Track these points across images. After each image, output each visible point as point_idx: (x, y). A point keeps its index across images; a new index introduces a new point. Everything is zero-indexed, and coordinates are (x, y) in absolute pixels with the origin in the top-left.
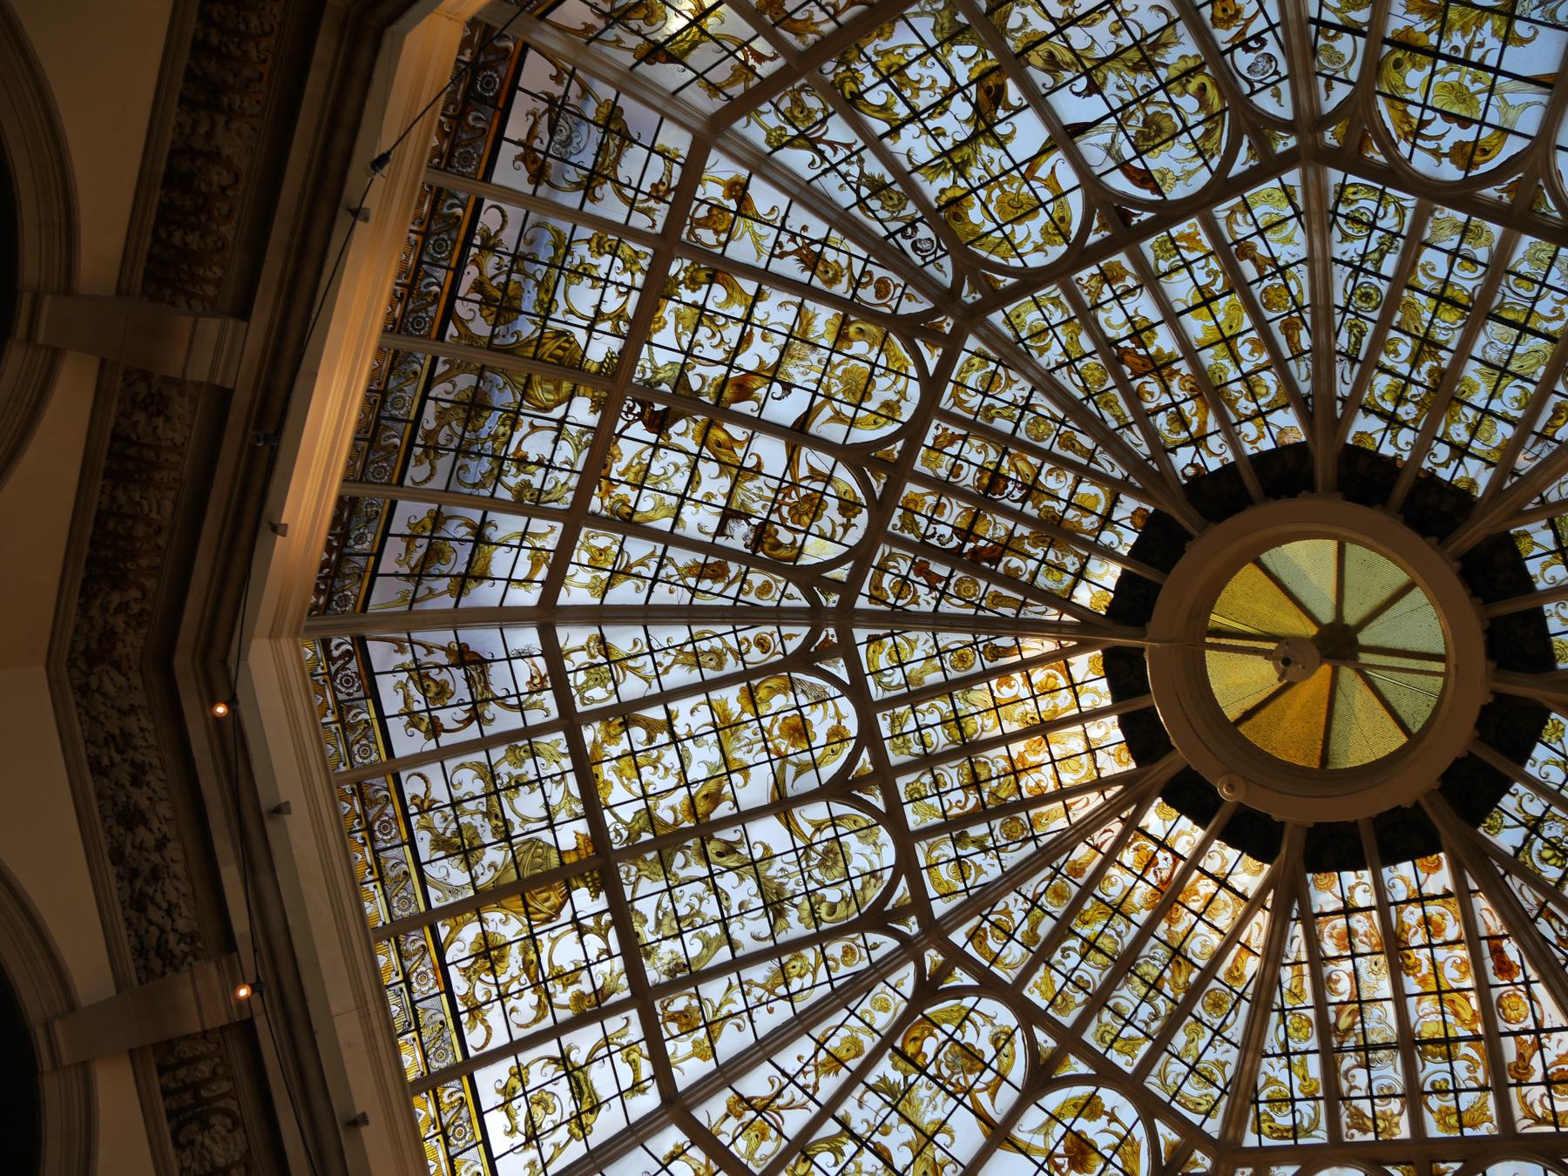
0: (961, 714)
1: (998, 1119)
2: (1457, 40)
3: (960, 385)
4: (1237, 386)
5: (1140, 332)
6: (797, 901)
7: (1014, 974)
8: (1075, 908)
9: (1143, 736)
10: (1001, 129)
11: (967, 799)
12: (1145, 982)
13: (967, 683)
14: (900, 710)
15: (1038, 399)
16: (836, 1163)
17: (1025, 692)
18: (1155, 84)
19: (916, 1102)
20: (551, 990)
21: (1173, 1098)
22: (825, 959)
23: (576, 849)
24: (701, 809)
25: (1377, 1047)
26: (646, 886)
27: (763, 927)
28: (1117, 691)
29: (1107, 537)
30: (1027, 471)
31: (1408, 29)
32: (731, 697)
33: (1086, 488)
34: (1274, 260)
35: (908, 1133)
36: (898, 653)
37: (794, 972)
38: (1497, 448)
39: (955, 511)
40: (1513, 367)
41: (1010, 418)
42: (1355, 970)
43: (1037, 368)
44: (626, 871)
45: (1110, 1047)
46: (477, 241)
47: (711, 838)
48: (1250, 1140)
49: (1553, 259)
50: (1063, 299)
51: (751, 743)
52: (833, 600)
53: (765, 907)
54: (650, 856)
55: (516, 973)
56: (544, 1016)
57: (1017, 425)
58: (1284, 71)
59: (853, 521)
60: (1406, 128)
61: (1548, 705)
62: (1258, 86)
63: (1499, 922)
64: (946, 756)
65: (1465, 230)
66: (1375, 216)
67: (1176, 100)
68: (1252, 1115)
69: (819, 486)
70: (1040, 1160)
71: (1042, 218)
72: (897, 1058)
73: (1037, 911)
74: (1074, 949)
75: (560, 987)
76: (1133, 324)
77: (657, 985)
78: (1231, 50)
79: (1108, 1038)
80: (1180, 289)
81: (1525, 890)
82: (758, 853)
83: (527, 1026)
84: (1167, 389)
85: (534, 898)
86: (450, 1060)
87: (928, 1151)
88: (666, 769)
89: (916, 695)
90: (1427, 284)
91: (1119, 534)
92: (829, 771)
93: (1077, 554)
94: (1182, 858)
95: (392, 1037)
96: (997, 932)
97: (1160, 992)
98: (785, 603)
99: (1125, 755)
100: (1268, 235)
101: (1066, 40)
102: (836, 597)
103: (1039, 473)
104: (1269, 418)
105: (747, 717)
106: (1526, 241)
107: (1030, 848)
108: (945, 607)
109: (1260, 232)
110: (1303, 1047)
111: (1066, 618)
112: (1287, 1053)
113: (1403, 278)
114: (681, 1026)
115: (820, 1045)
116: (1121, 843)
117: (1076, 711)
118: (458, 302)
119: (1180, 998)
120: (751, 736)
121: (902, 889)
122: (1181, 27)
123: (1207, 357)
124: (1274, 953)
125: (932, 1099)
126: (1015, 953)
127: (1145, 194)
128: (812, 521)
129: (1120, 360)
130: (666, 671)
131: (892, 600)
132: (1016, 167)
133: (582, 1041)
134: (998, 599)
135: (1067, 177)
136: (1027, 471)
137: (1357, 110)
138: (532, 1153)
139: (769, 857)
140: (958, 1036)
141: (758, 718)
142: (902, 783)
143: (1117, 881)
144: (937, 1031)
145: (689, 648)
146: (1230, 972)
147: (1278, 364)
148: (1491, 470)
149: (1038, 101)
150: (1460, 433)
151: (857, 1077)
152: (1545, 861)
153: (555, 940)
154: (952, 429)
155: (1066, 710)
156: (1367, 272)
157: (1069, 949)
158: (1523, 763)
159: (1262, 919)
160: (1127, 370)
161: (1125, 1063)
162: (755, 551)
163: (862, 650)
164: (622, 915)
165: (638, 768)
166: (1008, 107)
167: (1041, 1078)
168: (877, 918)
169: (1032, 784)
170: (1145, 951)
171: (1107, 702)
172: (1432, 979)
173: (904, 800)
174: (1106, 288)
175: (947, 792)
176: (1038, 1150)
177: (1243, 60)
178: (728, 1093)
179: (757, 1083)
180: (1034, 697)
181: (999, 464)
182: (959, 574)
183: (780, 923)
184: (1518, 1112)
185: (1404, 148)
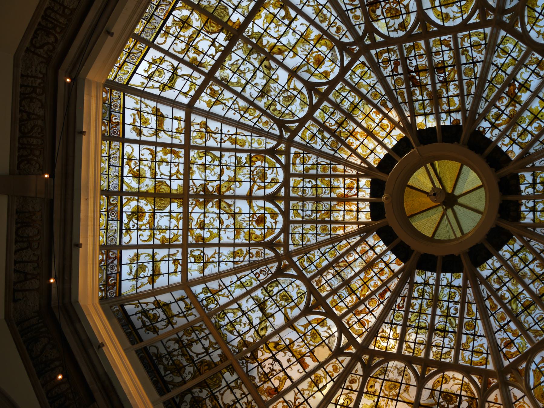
0: (358, 106)
5: (524, 86)
6: (269, 98)
8: (324, 176)
9: (386, 163)
11: (334, 125)
12: (317, 208)
13: (369, 102)
14: (347, 88)
15: (480, 65)
16: (210, 162)
17: (377, 121)
20: (190, 50)
21: (292, 234)
22: (260, 118)
23: (234, 23)
25: (340, 276)
26: (240, 52)
27: (255, 94)
28: (395, 148)
29: (443, 116)
30: (451, 77)
32: (315, 33)
33: (456, 100)
35: (232, 174)
36: (364, 74)
37: (250, 112)
38: (540, 220)
39: (423, 62)
41: (467, 60)
42: (357, 259)
43: (491, 58)
45: (293, 210)
46: (154, 358)
47: (268, 60)
48: (295, 259)
50: (523, 53)
51: (305, 50)
52: (368, 42)
53: (261, 91)
54: (249, 46)
55: (186, 36)
56: (182, 54)
59: (399, 31)
61: (464, 271)
63: (393, 288)
64: (342, 111)
68: (302, 255)
69: (403, 11)
70: (252, 212)
73: (315, 166)
75: (193, 51)
76: (526, 82)
79: (295, 208)
81: (407, 290)
82: (274, 77)
83: (175, 51)
84: (507, 106)
85: (210, 22)
86: (148, 38)
87: (231, 183)
88: (278, 30)
89: (355, 89)
91: (447, 119)
92: (314, 79)
93: (432, 110)
94: (358, 196)
95: (140, 17)
96: (302, 159)
97: (317, 213)
98: (357, 27)
99: (377, 162)
102: (369, 42)
103: (453, 81)
104: (514, 145)
105: (312, 42)
107: (332, 153)
108: (389, 79)
110: (328, 258)
111: (409, 119)
112: (323, 255)
115: (236, 134)
116: (351, 177)
117: (381, 140)
118: (165, 378)
119: (319, 219)
120: (307, 49)
123: (526, 114)
124: (347, 236)
125: (245, 174)
126: (300, 168)
128: (390, 17)
129: (510, 85)
130: (308, 6)
131: (380, 61)
133: (184, 70)
134: (402, 94)
136: (451, 77)
138: (146, 81)
139: (276, 81)
140: (267, 169)
141: (314, 46)
142: (325, 103)
143: (340, 183)
144: (264, 162)
145: (321, 7)
146: (335, 227)
148: (532, 222)
151: (236, 150)
152: (418, 291)
153: (204, 39)
155: (380, 137)
159: (355, 227)
160: (507, 90)
162: (367, 5)
163: (358, 62)
164: (227, 52)
165: (272, 21)
167: (272, 198)
169: (351, 141)
170: (325, 202)
172: (367, 280)
173: (321, 108)
175: (332, 119)
176: (253, 210)
178: (204, 119)
179: (213, 125)
180: (378, 125)
182: (402, 77)
183: (260, 98)
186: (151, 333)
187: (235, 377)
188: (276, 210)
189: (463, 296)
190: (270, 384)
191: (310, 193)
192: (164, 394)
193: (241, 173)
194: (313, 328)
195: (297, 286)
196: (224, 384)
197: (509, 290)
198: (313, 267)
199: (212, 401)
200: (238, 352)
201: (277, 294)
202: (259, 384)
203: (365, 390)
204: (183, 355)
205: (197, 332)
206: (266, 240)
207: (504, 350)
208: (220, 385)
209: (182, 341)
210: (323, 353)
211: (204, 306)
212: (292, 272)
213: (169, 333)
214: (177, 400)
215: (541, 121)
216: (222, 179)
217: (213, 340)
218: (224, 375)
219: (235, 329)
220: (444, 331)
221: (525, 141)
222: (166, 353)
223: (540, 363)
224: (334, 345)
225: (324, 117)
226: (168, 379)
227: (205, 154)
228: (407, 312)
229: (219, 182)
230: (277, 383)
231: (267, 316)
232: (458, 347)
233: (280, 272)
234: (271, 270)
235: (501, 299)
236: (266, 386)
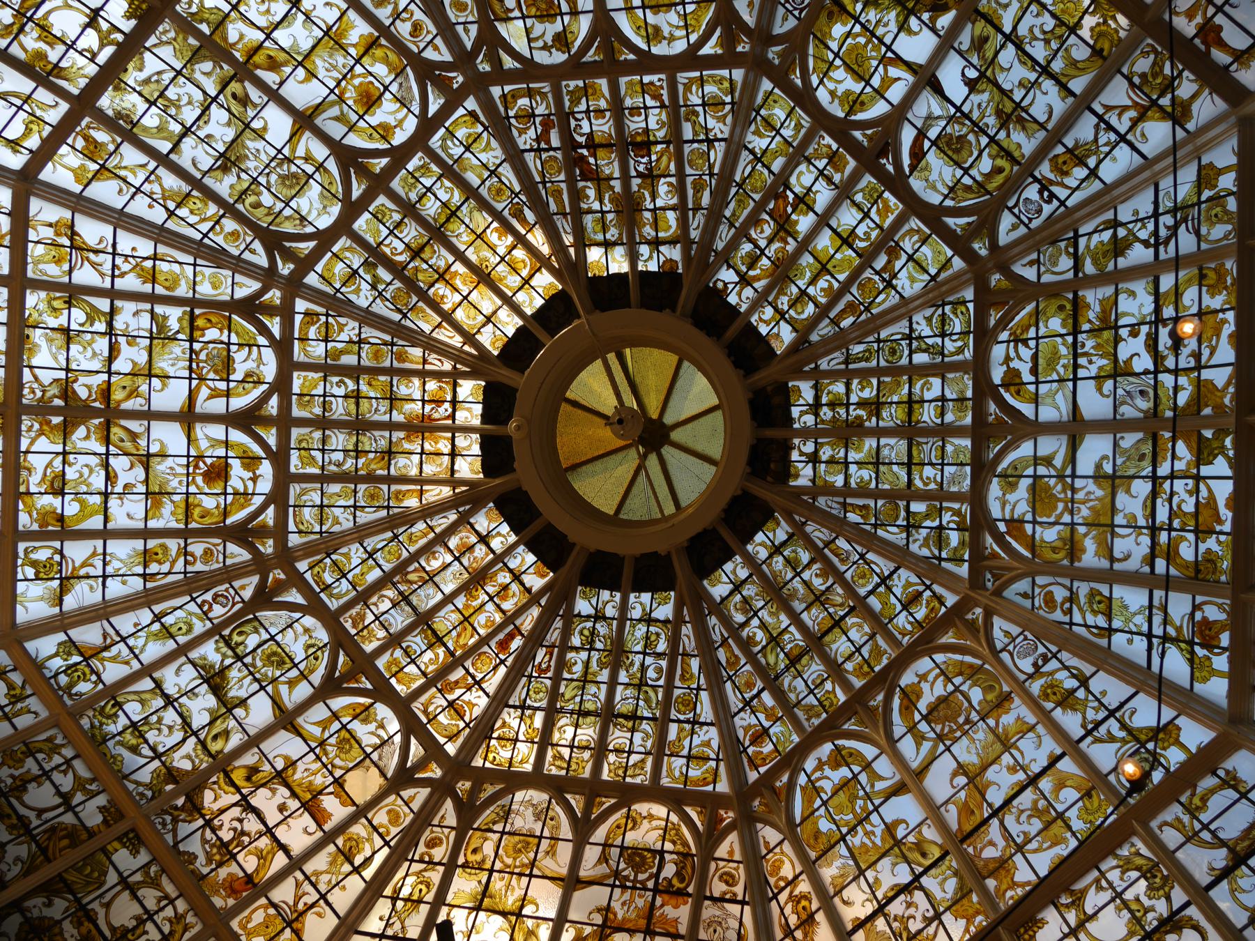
1: (198, 409)
3: (702, 81)
4: (795, 290)
6: (243, 175)
7: (302, 359)
8: (375, 371)
9: (519, 348)
10: (914, 23)
13: (484, 205)
14: (434, 167)
15: (720, 147)
16: (82, 325)
17: (502, 251)
18: (991, 132)
20: (27, 29)
22: (217, 222)
24: (258, 59)
25: (410, 604)
27: (206, 162)
28: (540, 314)
29: (644, 250)
30: (663, 166)
31: (1088, 306)
34: (895, 276)
35: (142, 358)
39: (604, 127)
40: (882, 468)
41: (695, 133)
44: (166, 28)
47: (241, 81)
48: (302, 566)
49: (962, 464)
50: (803, 131)
51: (335, 67)
52: (485, 67)
53: (222, 155)
54: (192, 41)
57: (692, 141)
58: (1034, 225)
62: (1016, 211)
64: (421, 221)
65: (961, 400)
67: (985, 154)
70: (193, 453)
71: (857, 87)
73: (356, 348)
75: (35, 34)
76: (807, 194)
77: (101, 111)
78: (1036, 180)
79: (304, 445)
80: (847, 217)
84: (770, 241)
87: (141, 379)
88: (268, 11)
89: (451, 172)
90: (917, 389)
91: (651, 257)
92: (354, 140)
98: (460, 29)
99: (500, 344)
100: (910, 264)
101: (1002, 46)
102: (488, 68)
106: (966, 443)
107: (396, 317)
108: (529, 157)
109: (910, 258)
110: (381, 562)
111: (572, 250)
114: (86, 148)
115: (155, 258)
116: (438, 375)
121: (306, 247)
122: (1042, 135)
123: (807, 259)
125: (177, 359)
126: (318, 350)
127: (906, 161)
129: (777, 197)
131: (511, 113)
132: (889, 48)
134: (557, 194)
135: (896, 93)
136: (663, 166)
137: (1022, 291)
139: (260, 135)
140: (234, 348)
141: (358, 61)
142: (382, 200)
143: (412, 388)
146: (399, 492)
147: (823, 311)
149: (946, 44)
150: (826, 453)
151: (153, 298)
152: (581, 633)
154: (664, 92)
156: (910, 345)
159: (446, 491)
160: (771, 206)
161: (295, 463)
163: (461, 111)
166: (933, 20)
167: (246, 420)
168: (274, 241)
169: (441, 292)
170: (377, 433)
171: (529, 311)
174: (825, 161)
176: (198, 448)
177: (1032, 192)
178: (67, 214)
179: (92, 231)
180: (503, 259)
181: (657, 143)
182: (559, 155)
183: (218, 174)
184: (423, 699)
185: (1004, 336)
188: (257, 450)
189: (674, 640)
190: (233, 868)
194: (344, 726)
195: (307, 630)
196: (112, 878)
198: (345, 585)
199: (78, 925)
200: (153, 798)
201: (254, 650)
202: (205, 871)
205: (40, 756)
206: (228, 522)
208: (103, 884)
210: (364, 785)
211: (60, 688)
212: (295, 597)
216: (114, 367)
217: (83, 772)
218: (114, 858)
219: (146, 741)
223: (814, 771)
225: (379, 231)
227: (69, 304)
228: (557, 680)
229: (105, 377)
231: (228, 706)
232: (660, 750)
236: (223, 873)
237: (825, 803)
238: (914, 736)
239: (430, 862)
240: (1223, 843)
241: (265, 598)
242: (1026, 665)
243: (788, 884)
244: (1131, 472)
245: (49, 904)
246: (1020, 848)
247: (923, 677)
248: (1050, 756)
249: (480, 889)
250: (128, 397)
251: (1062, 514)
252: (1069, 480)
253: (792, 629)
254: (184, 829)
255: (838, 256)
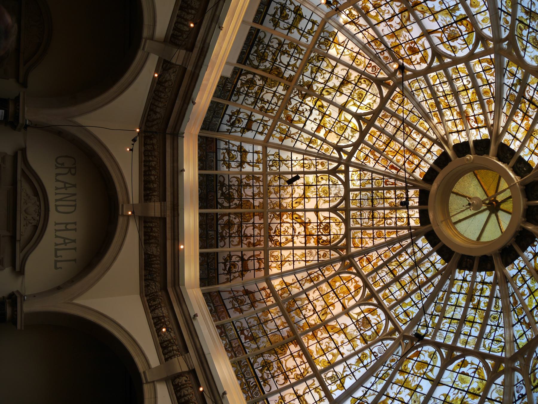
1: (431, 35)
2: (460, 396)
12: (448, 95)
19: (446, 16)
25: (397, 131)
28: (521, 159)
31: (473, 399)
46: (257, 40)
60: (479, 371)
66: (492, 343)
70: (415, 40)
72: (464, 16)
73: (486, 83)
74: (468, 84)
79: (439, 76)
87: (429, 12)
96: (488, 68)
97: (443, 96)
99: (506, 143)
100: (523, 332)
113: (484, 325)
119: (439, 99)
125: (445, 21)
126: (478, 69)
140: (462, 38)
143: (478, 110)
144: (467, 32)
152: (401, 194)
155: (529, 144)
157: (469, 83)
158: (419, 211)
169: (519, 115)
176: (418, 41)
183: (524, 11)
185: (481, 365)
186: (272, 24)
187: (284, 93)
188: (429, 60)
189: (402, 228)
190: (293, 115)
191: (458, 85)
192: (241, 63)
193: (443, 17)
194: (347, 126)
195: (375, 101)
196: (274, 89)
197: (406, 260)
198: (396, 107)
200: (301, 85)
201: (361, 88)
202: (289, 109)
203: (318, 175)
204: (274, 54)
207: (365, 258)
208: (271, 88)
209: (282, 46)
210: (333, 139)
211: (319, 41)
213: (281, 35)
214: (243, 72)
215: (528, 297)
218: (280, 86)
219: (316, 74)
220: (373, 217)
221: (517, 280)
222: (267, 44)
223: (355, 280)
224: (341, 144)
225: (534, 84)
226: (251, 57)
228: (383, 189)
230: (296, 119)
231: (339, 90)
232: (363, 229)
233: (380, 83)
234: (380, 74)
235: (399, 254)
236: (291, 113)
237: (344, 284)
238: (360, 313)
239: (316, 166)
240: (304, 394)
241: (380, 83)
242: (375, 349)
243: (323, 274)
244: (413, 397)
245: (259, 80)
246: (318, 342)
247: (379, 316)
248: (344, 353)
249: (310, 184)
250: (420, 11)
251: (414, 371)
252: (422, 376)
253: (403, 271)
254: (297, 98)
255: (534, 301)
